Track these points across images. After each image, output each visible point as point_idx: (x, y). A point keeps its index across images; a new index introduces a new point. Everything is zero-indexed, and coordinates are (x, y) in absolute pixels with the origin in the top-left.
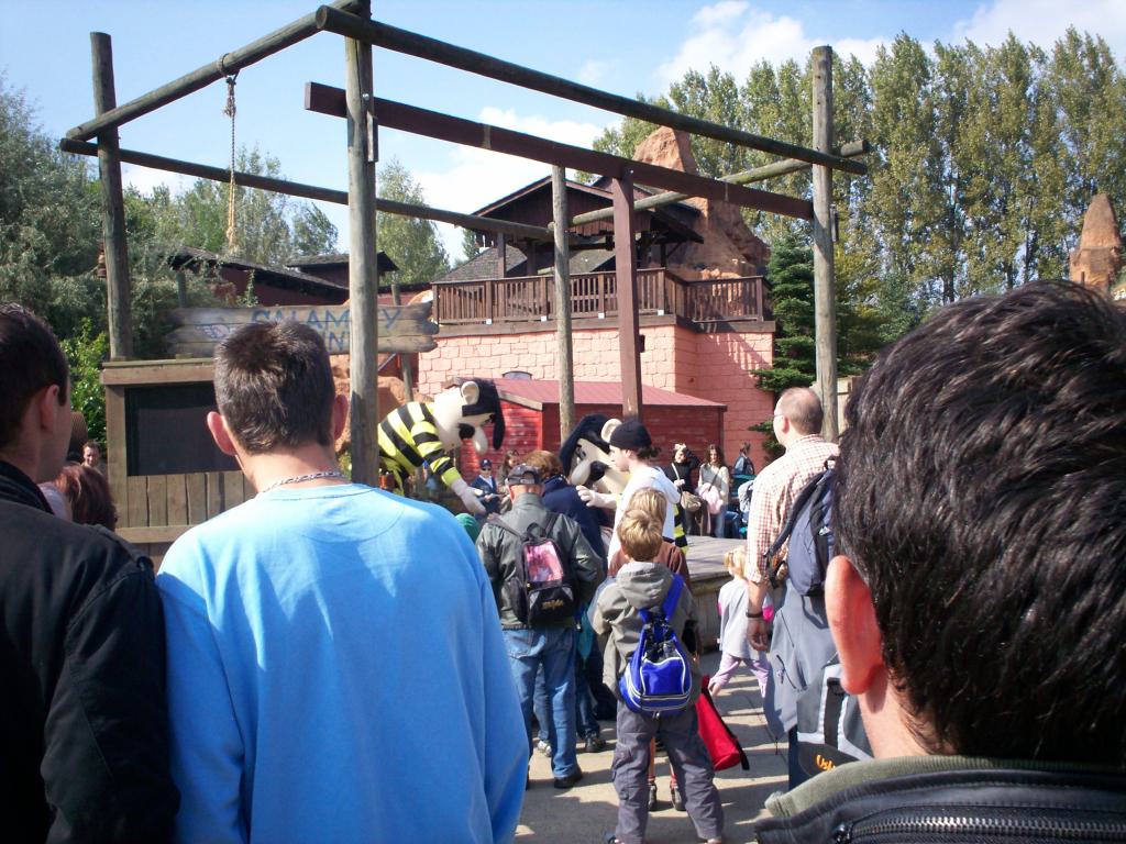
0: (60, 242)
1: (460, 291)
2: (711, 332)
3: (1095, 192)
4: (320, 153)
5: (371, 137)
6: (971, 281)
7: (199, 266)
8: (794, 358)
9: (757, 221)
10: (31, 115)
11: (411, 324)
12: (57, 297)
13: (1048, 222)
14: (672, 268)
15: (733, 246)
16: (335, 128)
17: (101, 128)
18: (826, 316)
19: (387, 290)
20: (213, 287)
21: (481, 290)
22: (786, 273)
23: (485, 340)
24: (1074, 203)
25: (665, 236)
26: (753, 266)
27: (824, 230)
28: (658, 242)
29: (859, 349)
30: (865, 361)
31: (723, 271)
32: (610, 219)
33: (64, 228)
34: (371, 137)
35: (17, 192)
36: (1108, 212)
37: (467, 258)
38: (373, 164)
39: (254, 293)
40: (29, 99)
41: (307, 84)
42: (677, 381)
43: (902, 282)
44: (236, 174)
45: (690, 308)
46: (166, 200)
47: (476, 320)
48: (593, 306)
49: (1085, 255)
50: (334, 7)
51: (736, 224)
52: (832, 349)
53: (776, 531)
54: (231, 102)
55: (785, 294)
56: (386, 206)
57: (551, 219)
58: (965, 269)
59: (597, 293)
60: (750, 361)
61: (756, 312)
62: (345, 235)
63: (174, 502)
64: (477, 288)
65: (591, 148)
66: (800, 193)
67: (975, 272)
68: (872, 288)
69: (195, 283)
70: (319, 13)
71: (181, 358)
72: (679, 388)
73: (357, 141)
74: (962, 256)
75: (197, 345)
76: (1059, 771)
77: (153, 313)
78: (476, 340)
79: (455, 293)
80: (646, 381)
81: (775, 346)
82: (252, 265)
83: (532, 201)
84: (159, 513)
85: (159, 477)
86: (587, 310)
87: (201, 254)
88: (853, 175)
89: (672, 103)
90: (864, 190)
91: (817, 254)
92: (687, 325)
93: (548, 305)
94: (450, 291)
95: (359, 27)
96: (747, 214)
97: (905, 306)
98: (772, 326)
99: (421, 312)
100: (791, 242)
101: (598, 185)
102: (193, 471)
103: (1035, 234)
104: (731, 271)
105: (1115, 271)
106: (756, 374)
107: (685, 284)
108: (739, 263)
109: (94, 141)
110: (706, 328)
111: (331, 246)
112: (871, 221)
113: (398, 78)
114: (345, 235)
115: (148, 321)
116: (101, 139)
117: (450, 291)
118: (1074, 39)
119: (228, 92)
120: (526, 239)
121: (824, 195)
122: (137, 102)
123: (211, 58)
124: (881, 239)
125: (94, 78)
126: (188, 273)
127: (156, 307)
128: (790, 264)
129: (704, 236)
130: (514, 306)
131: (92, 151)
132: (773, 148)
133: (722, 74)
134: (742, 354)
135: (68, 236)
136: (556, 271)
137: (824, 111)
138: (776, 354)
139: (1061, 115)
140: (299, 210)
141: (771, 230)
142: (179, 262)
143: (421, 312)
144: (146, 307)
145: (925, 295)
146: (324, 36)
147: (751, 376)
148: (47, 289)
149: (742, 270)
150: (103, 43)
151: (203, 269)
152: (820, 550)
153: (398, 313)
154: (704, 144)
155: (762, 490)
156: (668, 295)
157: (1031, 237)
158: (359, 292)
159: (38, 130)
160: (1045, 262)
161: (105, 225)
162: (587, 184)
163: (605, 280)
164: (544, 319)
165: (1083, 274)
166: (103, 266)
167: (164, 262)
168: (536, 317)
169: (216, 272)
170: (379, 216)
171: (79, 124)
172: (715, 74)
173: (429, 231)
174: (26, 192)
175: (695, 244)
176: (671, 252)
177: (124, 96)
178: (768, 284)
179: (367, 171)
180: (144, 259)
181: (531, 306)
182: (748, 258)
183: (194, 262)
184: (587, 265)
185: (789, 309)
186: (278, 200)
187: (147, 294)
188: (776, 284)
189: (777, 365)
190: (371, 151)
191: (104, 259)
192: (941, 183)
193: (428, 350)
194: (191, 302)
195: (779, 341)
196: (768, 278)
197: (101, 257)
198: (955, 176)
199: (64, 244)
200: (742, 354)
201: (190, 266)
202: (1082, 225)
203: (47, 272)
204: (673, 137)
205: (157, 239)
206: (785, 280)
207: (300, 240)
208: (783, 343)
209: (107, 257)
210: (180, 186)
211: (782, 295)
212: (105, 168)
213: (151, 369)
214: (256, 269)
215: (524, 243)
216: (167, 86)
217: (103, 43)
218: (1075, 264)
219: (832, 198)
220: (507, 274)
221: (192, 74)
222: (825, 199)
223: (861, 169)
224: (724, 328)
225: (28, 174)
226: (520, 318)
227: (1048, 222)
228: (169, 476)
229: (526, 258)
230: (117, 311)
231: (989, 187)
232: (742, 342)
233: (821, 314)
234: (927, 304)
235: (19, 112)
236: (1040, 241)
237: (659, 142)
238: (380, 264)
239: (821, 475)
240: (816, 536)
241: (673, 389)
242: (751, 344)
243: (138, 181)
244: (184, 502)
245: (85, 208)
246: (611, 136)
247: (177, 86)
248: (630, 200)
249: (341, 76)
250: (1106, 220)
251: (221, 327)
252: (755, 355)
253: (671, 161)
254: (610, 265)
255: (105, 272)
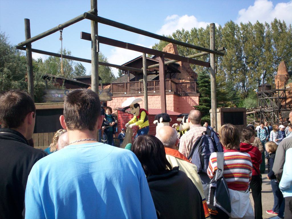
0: (14, 72)
1: (118, 85)
2: (183, 96)
3: (281, 61)
4: (84, 50)
5: (97, 46)
6: (249, 83)
7: (50, 79)
8: (204, 103)
9: (194, 68)
10: (7, 39)
11: (106, 94)
12: (12, 86)
13: (269, 68)
14: (172, 79)
15: (188, 74)
16: (88, 43)
17: (26, 43)
18: (214, 92)
19: (100, 85)
20: (54, 84)
21: (123, 85)
22: (202, 81)
23: (124, 98)
24: (276, 63)
25: (171, 71)
26: (193, 79)
27: (213, 70)
28: (169, 73)
29: (221, 101)
30: (222, 104)
31: (185, 80)
32: (158, 67)
33: (15, 68)
34: (97, 46)
35: (3, 59)
36: (284, 66)
37: (119, 77)
38: (98, 53)
39: (64, 85)
40: (6, 36)
41: (81, 32)
42: (174, 109)
43: (231, 83)
44: (63, 55)
45: (177, 90)
46: (42, 61)
47: (122, 93)
48: (152, 89)
49: (278, 77)
50: (88, 13)
51: (189, 68)
52: (215, 100)
53: (188, 154)
54: (61, 37)
55: (202, 86)
56: (102, 64)
57: (142, 67)
58: (248, 80)
59: (153, 86)
60: (193, 103)
61: (194, 91)
62: (89, 70)
63: (45, 140)
64: (122, 84)
65: (151, 48)
66: (205, 60)
67: (251, 81)
68: (224, 85)
69: (49, 83)
70: (84, 14)
71: (48, 102)
72: (175, 110)
73: (94, 47)
74: (247, 77)
75: (50, 99)
76: (289, 144)
77: (38, 91)
78: (122, 98)
79: (117, 86)
80: (167, 109)
81: (199, 100)
82: (64, 78)
83: (138, 62)
84: (41, 143)
85: (42, 133)
86: (151, 90)
87: (51, 75)
88: (218, 56)
89: (173, 37)
90: (221, 59)
91: (211, 76)
92: (177, 94)
93: (141, 89)
94: (115, 85)
95: (93, 17)
96: (192, 66)
97: (232, 89)
98: (199, 94)
99: (108, 91)
100: (203, 73)
101: (153, 58)
102: (50, 132)
103: (266, 71)
104: (188, 80)
105: (287, 80)
106: (195, 107)
107: (176, 84)
108: (189, 78)
109: (25, 46)
110: (181, 95)
111: (84, 73)
112: (223, 68)
113: (105, 31)
114: (89, 70)
115: (37, 93)
116: (27, 46)
117: (115, 85)
118: (276, 21)
119: (60, 34)
120: (135, 72)
121: (213, 61)
122: (37, 36)
123: (56, 25)
124: (226, 72)
125: (25, 30)
126: (48, 80)
127: (39, 89)
128: (203, 79)
129: (181, 71)
130: (132, 89)
131: (24, 49)
132: (199, 49)
133: (185, 30)
134: (191, 102)
135: (16, 71)
136: (144, 80)
137: (213, 40)
138: (200, 102)
139: (272, 41)
140: (76, 64)
141: (198, 70)
142: (44, 77)
143: (108, 91)
144: (36, 89)
145: (237, 87)
146: (86, 20)
147: (193, 107)
148: (10, 84)
149: (190, 80)
150: (28, 21)
151: (51, 79)
152: (202, 160)
153: (102, 91)
154: (181, 48)
155: (183, 141)
156: (172, 86)
157: (265, 72)
158: (94, 85)
159: (9, 43)
160: (268, 79)
161: (28, 68)
162: (150, 58)
163: (156, 82)
164: (140, 92)
165: (278, 82)
166: (27, 79)
167: (41, 77)
168: (138, 92)
169: (55, 80)
170: (99, 66)
171: (21, 42)
172: (183, 31)
173: (109, 70)
174: (5, 59)
175: (178, 73)
176: (172, 75)
177: (33, 35)
178: (197, 84)
179: (96, 54)
180: (36, 77)
181: (136, 89)
182: (192, 77)
183: (49, 77)
184: (150, 79)
185: (203, 90)
186: (71, 62)
187: (36, 86)
188: (200, 84)
189: (200, 105)
190: (97, 49)
191: (27, 77)
192: (241, 58)
193: (110, 100)
194: (48, 88)
195: (201, 98)
196: (197, 82)
197: (26, 76)
198: (245, 56)
199: (15, 73)
200: (191, 102)
201: (48, 79)
202: (278, 69)
203: (11, 80)
204: (173, 46)
205: (39, 72)
206: (202, 83)
207: (76, 72)
208: (201, 99)
209: (28, 76)
210: (45, 58)
211: (202, 87)
212: (28, 53)
213: (40, 105)
214: (65, 79)
215: (135, 73)
216: (44, 32)
217: (28, 21)
218: (276, 79)
219: (215, 62)
220: (130, 81)
221: (51, 29)
222: (213, 62)
223: (222, 55)
224: (186, 95)
225: (6, 55)
226: (133, 92)
227: (269, 68)
228: (45, 133)
229: (135, 77)
230: (30, 90)
231: (254, 59)
232: (191, 99)
233: (212, 92)
234: (238, 89)
235: (3, 38)
236: (267, 73)
237: (169, 47)
238: (98, 78)
239: (201, 137)
240: (200, 156)
241: (173, 111)
242: (193, 99)
243: (36, 56)
244: (48, 140)
245: (21, 64)
246: (157, 45)
247: (47, 32)
248: (163, 62)
249: (90, 30)
250: (284, 68)
251: (57, 94)
252: (195, 102)
253: (172, 52)
254: (157, 78)
255: (27, 80)
